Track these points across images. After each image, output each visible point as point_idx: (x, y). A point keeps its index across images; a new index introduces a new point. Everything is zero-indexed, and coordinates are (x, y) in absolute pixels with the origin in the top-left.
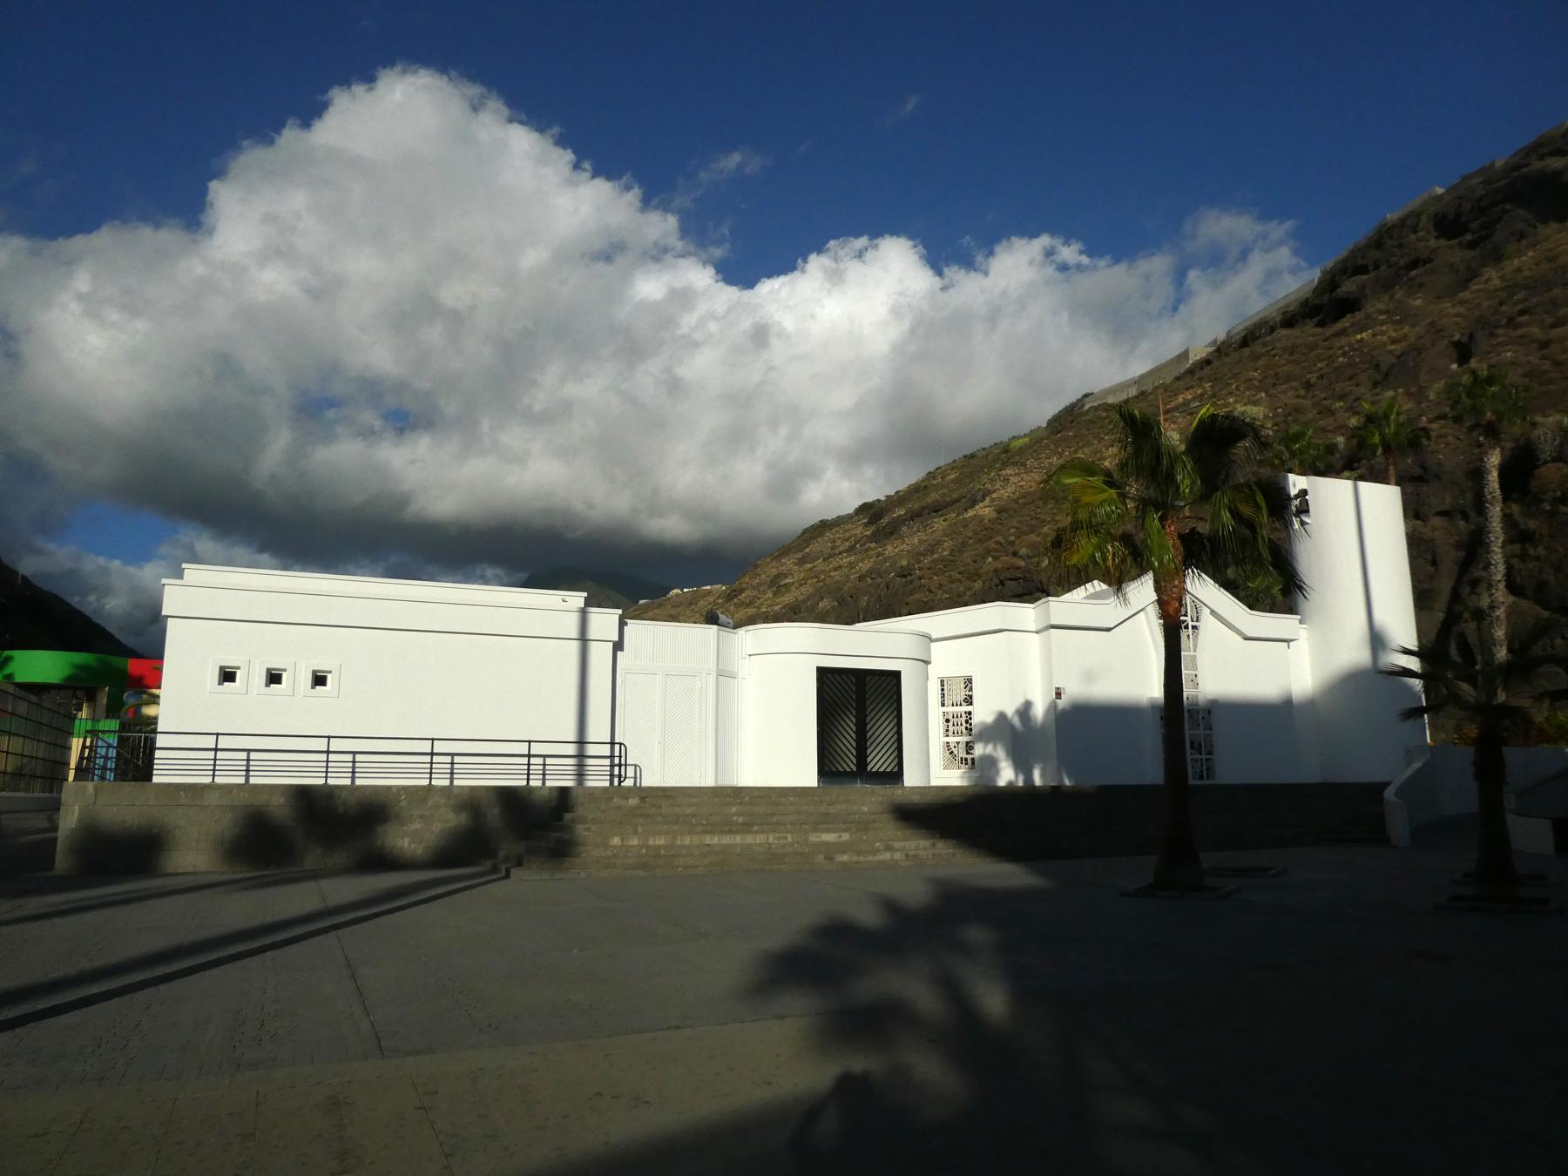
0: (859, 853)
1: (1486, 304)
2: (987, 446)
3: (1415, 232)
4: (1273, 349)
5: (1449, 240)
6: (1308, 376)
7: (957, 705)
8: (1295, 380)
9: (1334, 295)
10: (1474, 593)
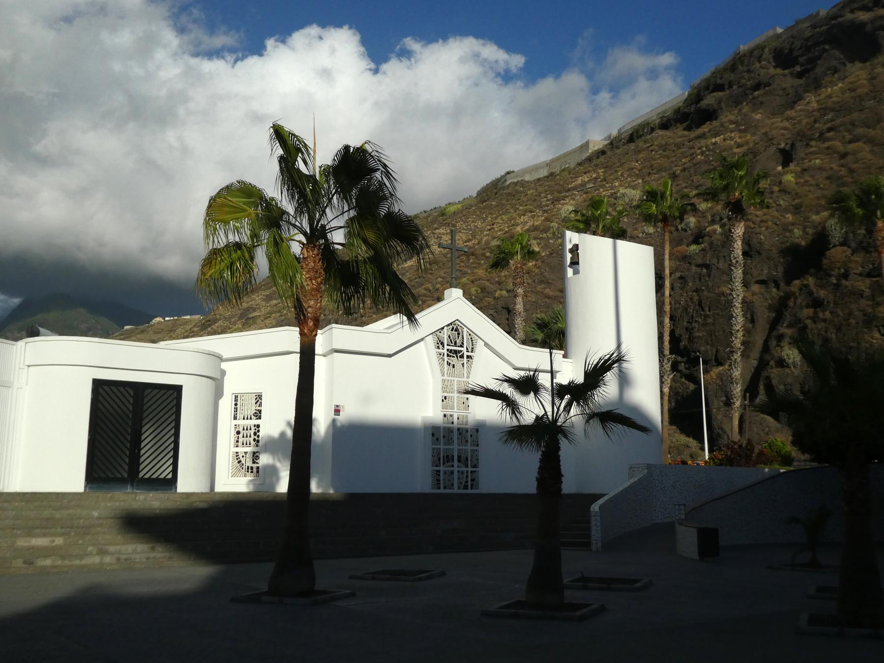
0: (63, 558)
1: (805, 121)
2: (428, 209)
3: (760, 62)
4: (652, 145)
5: (784, 70)
6: (675, 169)
7: (247, 419)
8: (665, 171)
9: (698, 106)
10: (778, 345)
